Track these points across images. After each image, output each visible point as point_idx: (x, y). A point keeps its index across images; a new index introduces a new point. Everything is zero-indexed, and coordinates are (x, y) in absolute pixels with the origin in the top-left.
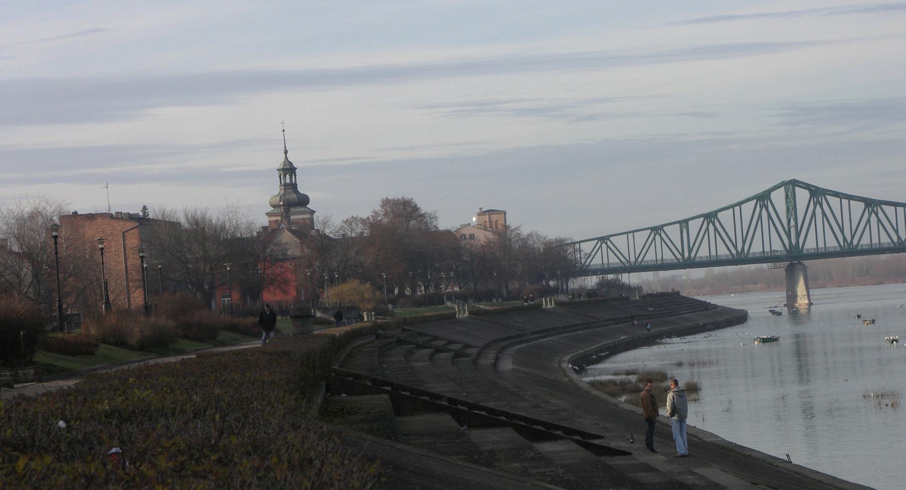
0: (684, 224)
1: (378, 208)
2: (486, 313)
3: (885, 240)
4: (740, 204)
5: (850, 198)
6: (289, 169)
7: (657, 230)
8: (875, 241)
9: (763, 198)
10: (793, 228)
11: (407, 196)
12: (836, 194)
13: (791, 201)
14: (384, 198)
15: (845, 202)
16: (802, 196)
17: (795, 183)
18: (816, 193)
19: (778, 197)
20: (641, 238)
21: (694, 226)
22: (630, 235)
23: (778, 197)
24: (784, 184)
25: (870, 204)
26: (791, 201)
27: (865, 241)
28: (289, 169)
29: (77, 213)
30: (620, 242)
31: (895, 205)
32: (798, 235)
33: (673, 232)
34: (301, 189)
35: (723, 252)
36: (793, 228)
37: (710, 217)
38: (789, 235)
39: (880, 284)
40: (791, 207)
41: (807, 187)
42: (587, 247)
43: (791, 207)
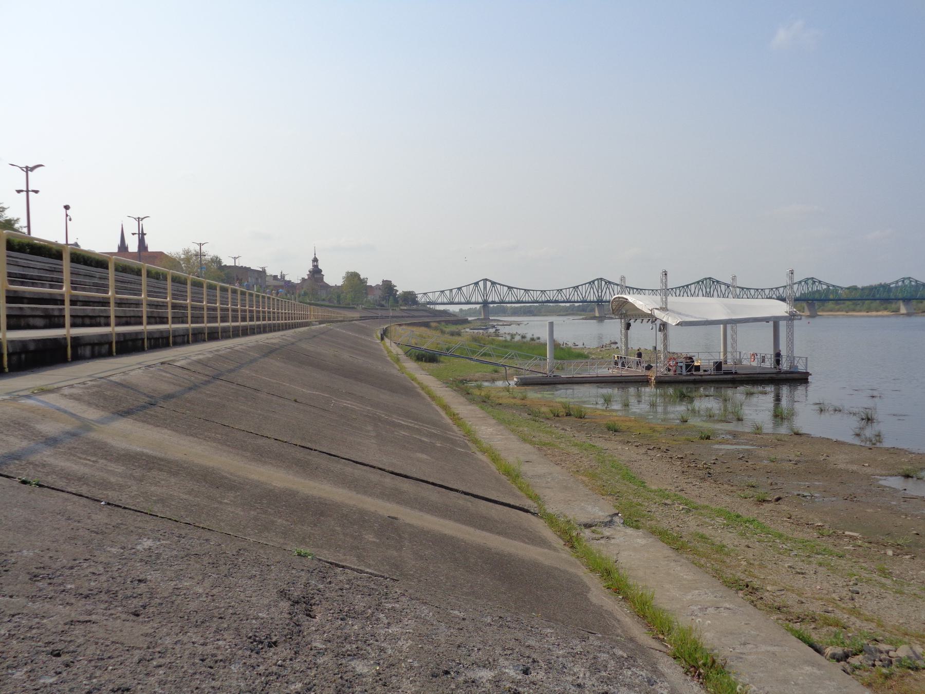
0: (451, 290)
1: (181, 252)
2: (404, 310)
3: (513, 300)
4: (469, 285)
5: (503, 285)
6: (315, 260)
7: (442, 292)
8: (510, 300)
9: (477, 284)
10: (485, 294)
11: (356, 271)
12: (499, 284)
13: (600, 286)
14: (187, 248)
15: (616, 286)
16: (489, 284)
17: (486, 280)
18: (493, 283)
19: (481, 284)
20: (437, 294)
21: (454, 291)
22: (584, 286)
23: (481, 284)
24: (597, 279)
25: (510, 288)
26: (600, 286)
27: (507, 300)
28: (315, 260)
29: (363, 282)
30: (430, 295)
31: (517, 289)
32: (487, 296)
33: (448, 293)
34: (319, 267)
35: (463, 300)
36: (485, 294)
37: (460, 289)
38: (484, 296)
39: (837, 442)
40: (485, 287)
41: (490, 281)
42: (419, 296)
43: (485, 287)
